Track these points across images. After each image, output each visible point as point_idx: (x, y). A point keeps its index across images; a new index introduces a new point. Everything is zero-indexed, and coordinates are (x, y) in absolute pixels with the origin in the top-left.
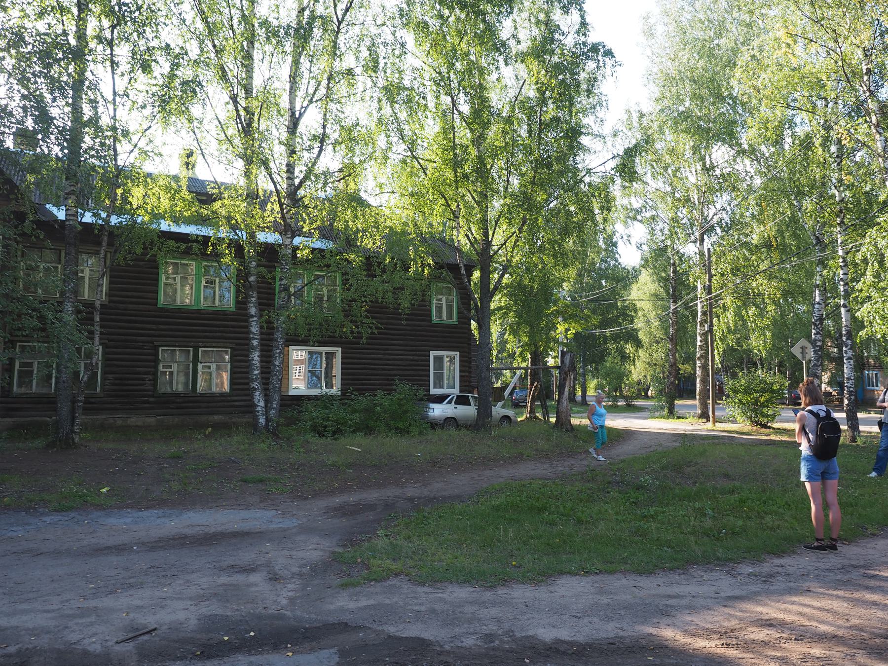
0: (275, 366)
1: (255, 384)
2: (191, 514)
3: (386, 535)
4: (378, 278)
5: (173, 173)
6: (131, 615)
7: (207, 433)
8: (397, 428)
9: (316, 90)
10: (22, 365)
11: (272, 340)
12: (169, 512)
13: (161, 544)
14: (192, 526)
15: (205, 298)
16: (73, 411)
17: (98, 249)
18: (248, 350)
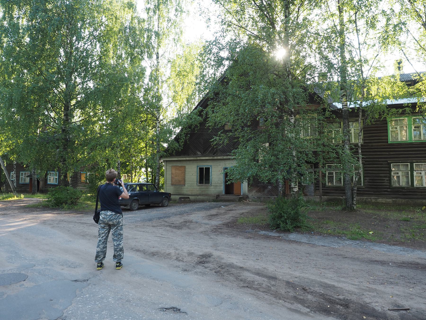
5: (391, 74)
6: (395, 298)
7: (423, 209)
10: (329, 173)
12: (406, 249)
13: (404, 265)
14: (421, 259)
16: (352, 195)
17: (358, 119)
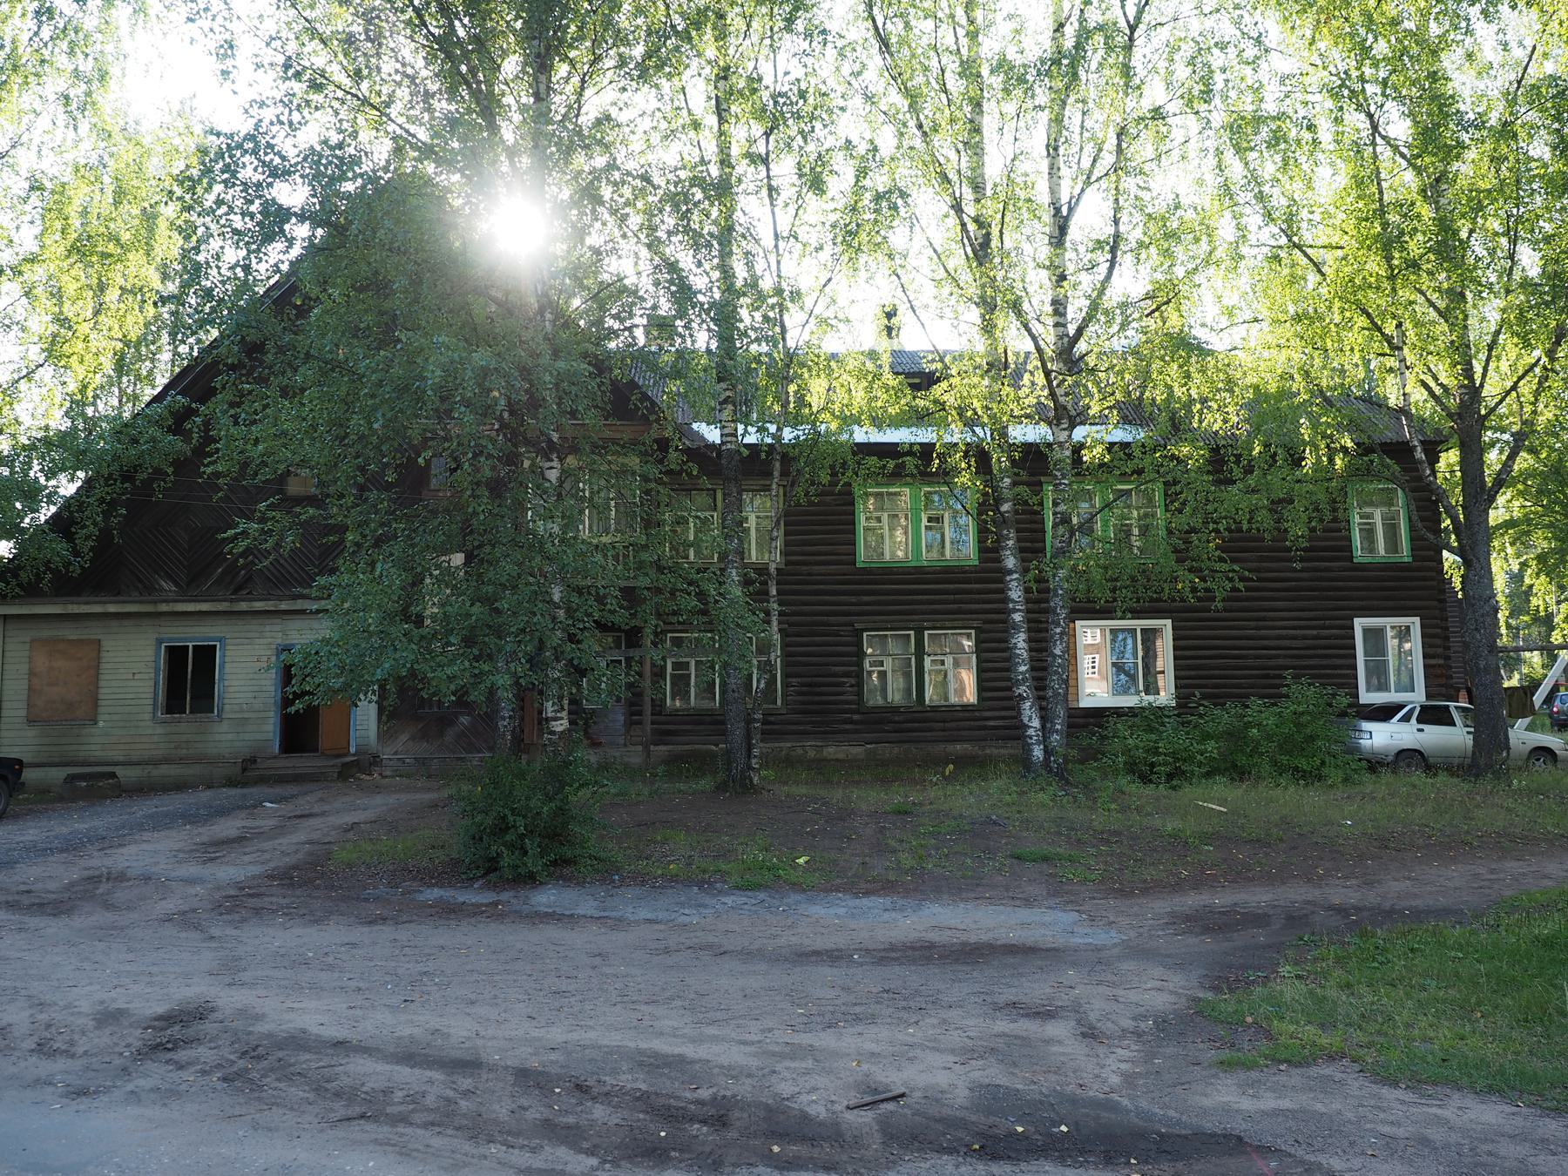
0: (1055, 656)
1: (1022, 690)
2: (936, 908)
3: (1298, 977)
4: (1240, 485)
5: (866, 348)
8: (1296, 769)
9: (1095, 161)
10: (676, 666)
11: (1046, 611)
12: (901, 902)
15: (929, 547)
16: (748, 736)
17: (768, 483)
18: (1006, 631)
